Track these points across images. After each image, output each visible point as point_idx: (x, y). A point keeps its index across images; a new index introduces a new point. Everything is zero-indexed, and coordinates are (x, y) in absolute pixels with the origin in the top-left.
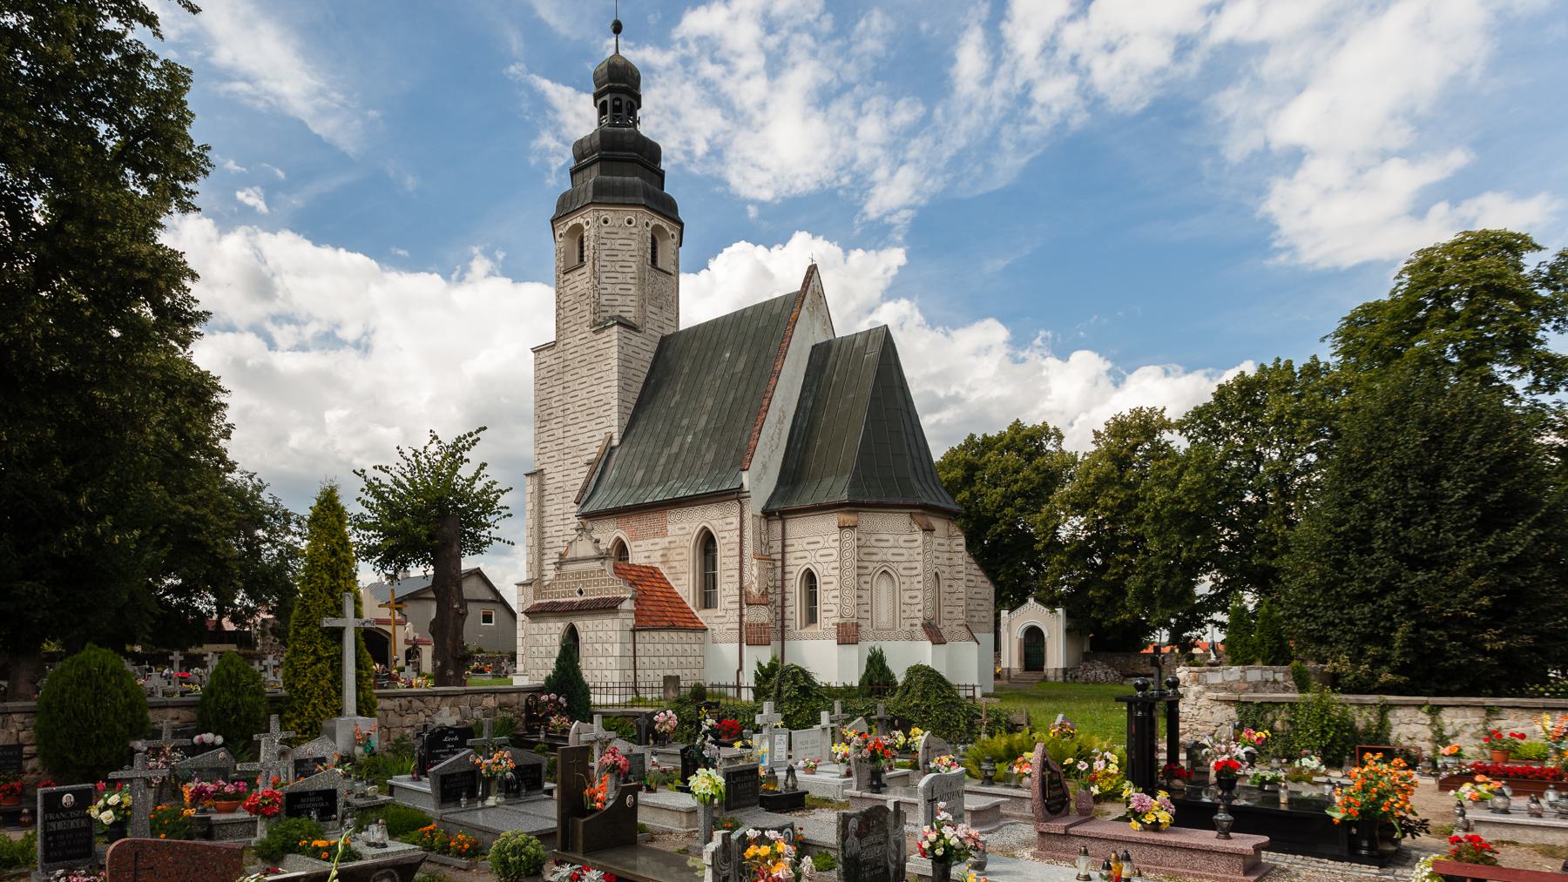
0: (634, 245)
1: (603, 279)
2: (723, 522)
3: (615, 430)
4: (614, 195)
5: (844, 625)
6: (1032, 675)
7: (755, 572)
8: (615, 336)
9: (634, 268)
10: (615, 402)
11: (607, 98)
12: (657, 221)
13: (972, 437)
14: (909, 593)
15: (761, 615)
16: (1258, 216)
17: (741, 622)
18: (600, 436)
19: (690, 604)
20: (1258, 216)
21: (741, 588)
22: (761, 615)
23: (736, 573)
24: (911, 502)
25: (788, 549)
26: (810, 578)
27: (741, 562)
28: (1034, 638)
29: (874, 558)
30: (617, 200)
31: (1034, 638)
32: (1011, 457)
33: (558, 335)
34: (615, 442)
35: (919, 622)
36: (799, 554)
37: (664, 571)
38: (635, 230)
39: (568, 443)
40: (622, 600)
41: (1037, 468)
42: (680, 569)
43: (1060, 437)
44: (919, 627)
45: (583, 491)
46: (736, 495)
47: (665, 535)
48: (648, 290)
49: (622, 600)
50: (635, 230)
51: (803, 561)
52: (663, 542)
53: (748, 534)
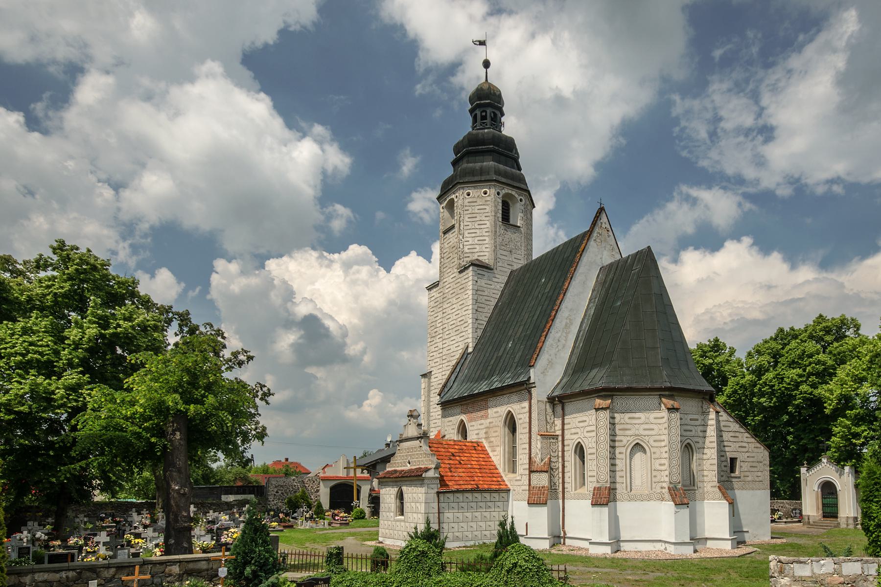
0: (488, 208)
1: (466, 235)
2: (519, 409)
3: (470, 340)
4: (473, 176)
5: (599, 489)
6: (829, 521)
7: (539, 446)
8: (471, 274)
9: (488, 225)
10: (470, 321)
11: (478, 112)
12: (507, 190)
13: (782, 330)
14: (658, 462)
15: (542, 480)
16: (419, 158)
17: (530, 484)
18: (462, 346)
19: (501, 470)
20: (419, 158)
21: (530, 458)
22: (542, 480)
23: (527, 446)
24: (657, 386)
25: (566, 427)
26: (580, 451)
27: (530, 438)
28: (828, 490)
29: (628, 433)
30: (476, 179)
31: (828, 490)
32: (811, 346)
33: (440, 277)
34: (470, 350)
35: (665, 485)
36: (573, 431)
37: (486, 445)
38: (488, 199)
39: (445, 352)
40: (427, 470)
41: (830, 352)
42: (495, 443)
43: (857, 327)
44: (667, 490)
45: (445, 386)
46: (523, 388)
47: (487, 417)
48: (499, 240)
49: (427, 470)
50: (488, 199)
51: (575, 437)
52: (486, 422)
53: (534, 415)
